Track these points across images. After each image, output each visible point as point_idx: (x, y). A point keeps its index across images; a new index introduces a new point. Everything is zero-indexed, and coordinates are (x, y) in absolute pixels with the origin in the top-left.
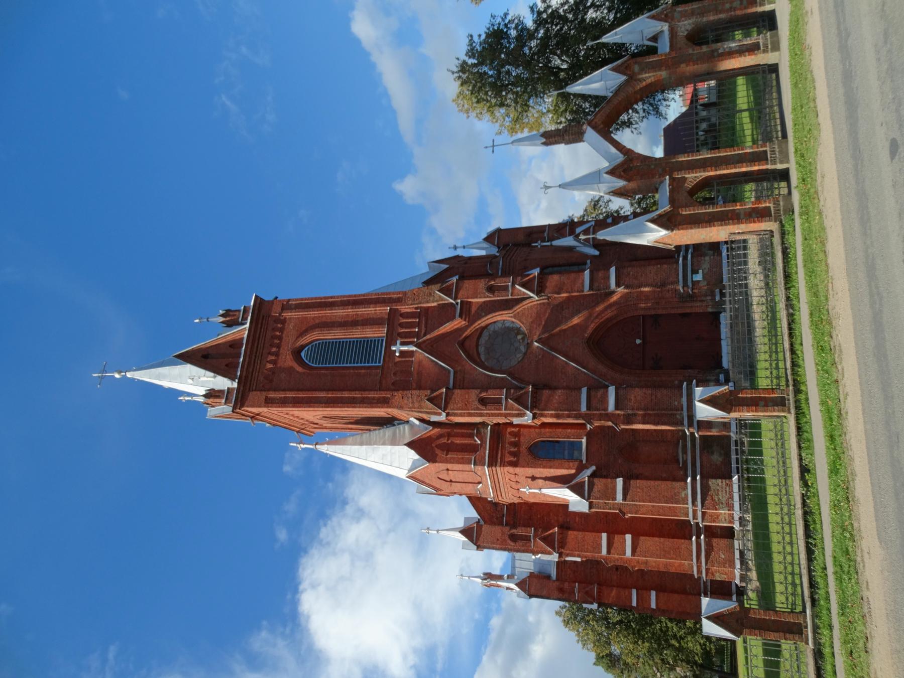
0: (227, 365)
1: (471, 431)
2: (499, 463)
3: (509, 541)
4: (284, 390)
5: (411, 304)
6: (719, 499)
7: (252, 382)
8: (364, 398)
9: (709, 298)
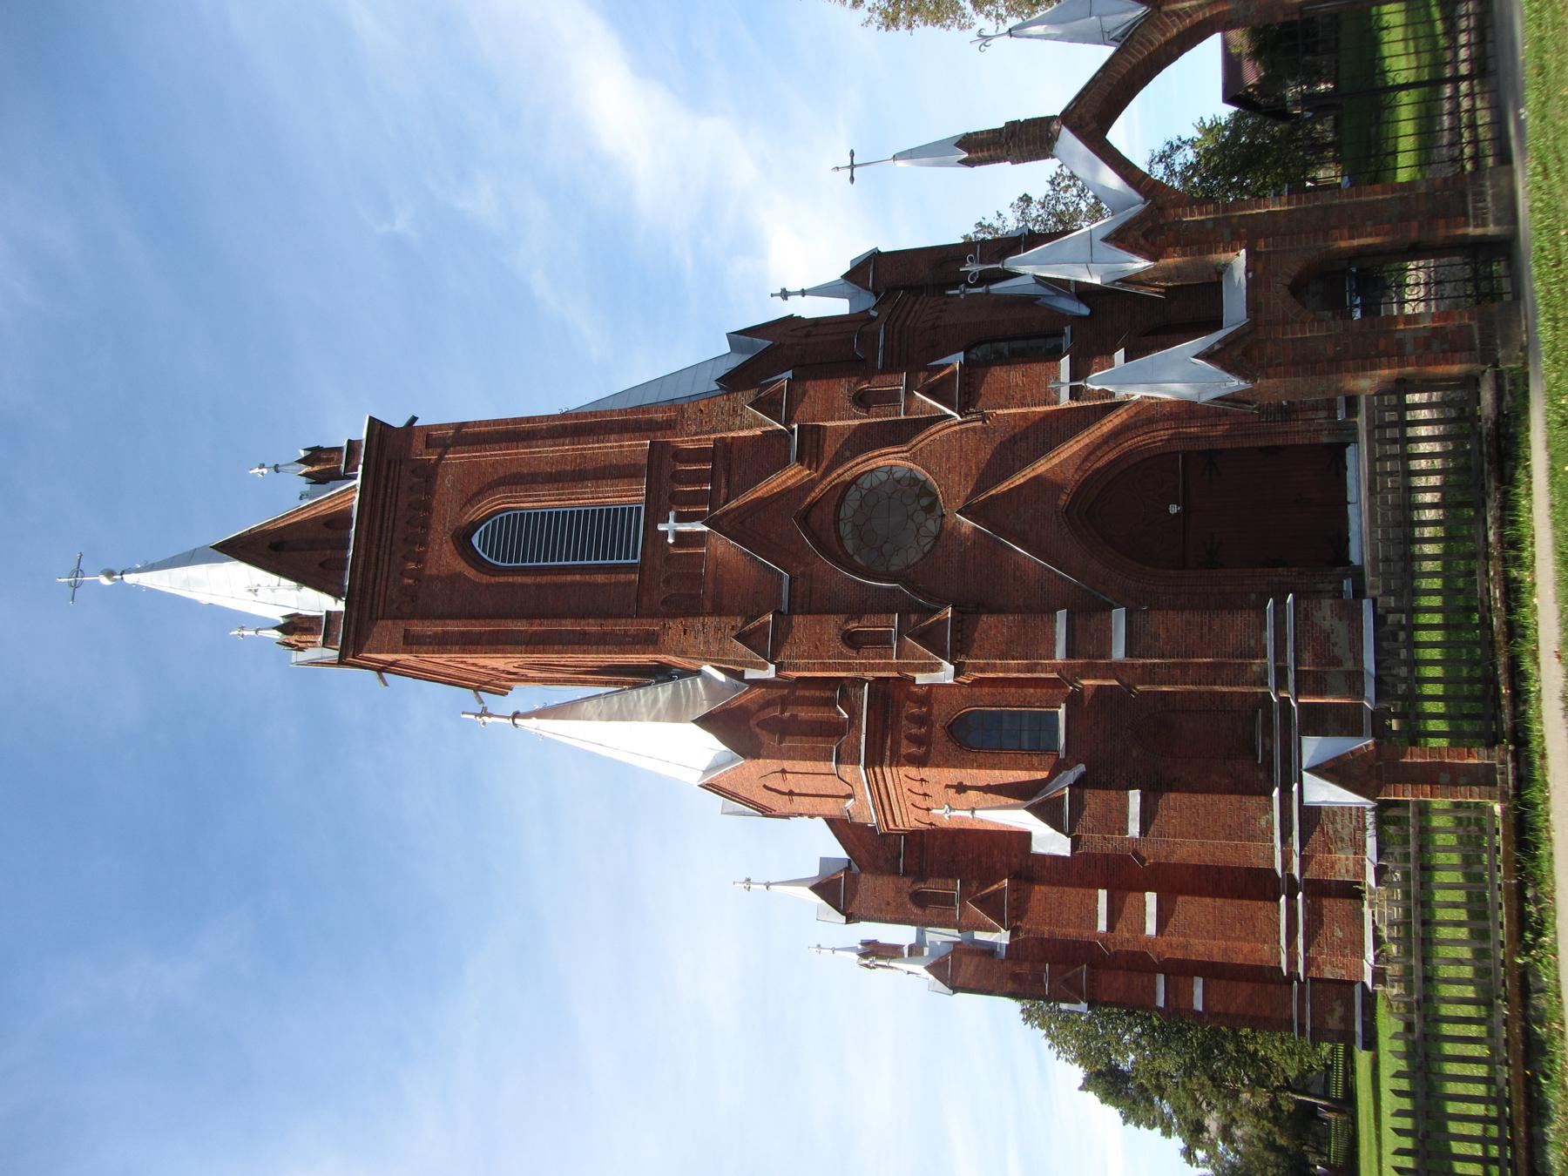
0: (321, 565)
1: (828, 694)
2: (887, 761)
3: (910, 906)
4: (442, 617)
5: (696, 434)
6: (1336, 831)
7: (375, 602)
8: (605, 633)
9: (1323, 414)
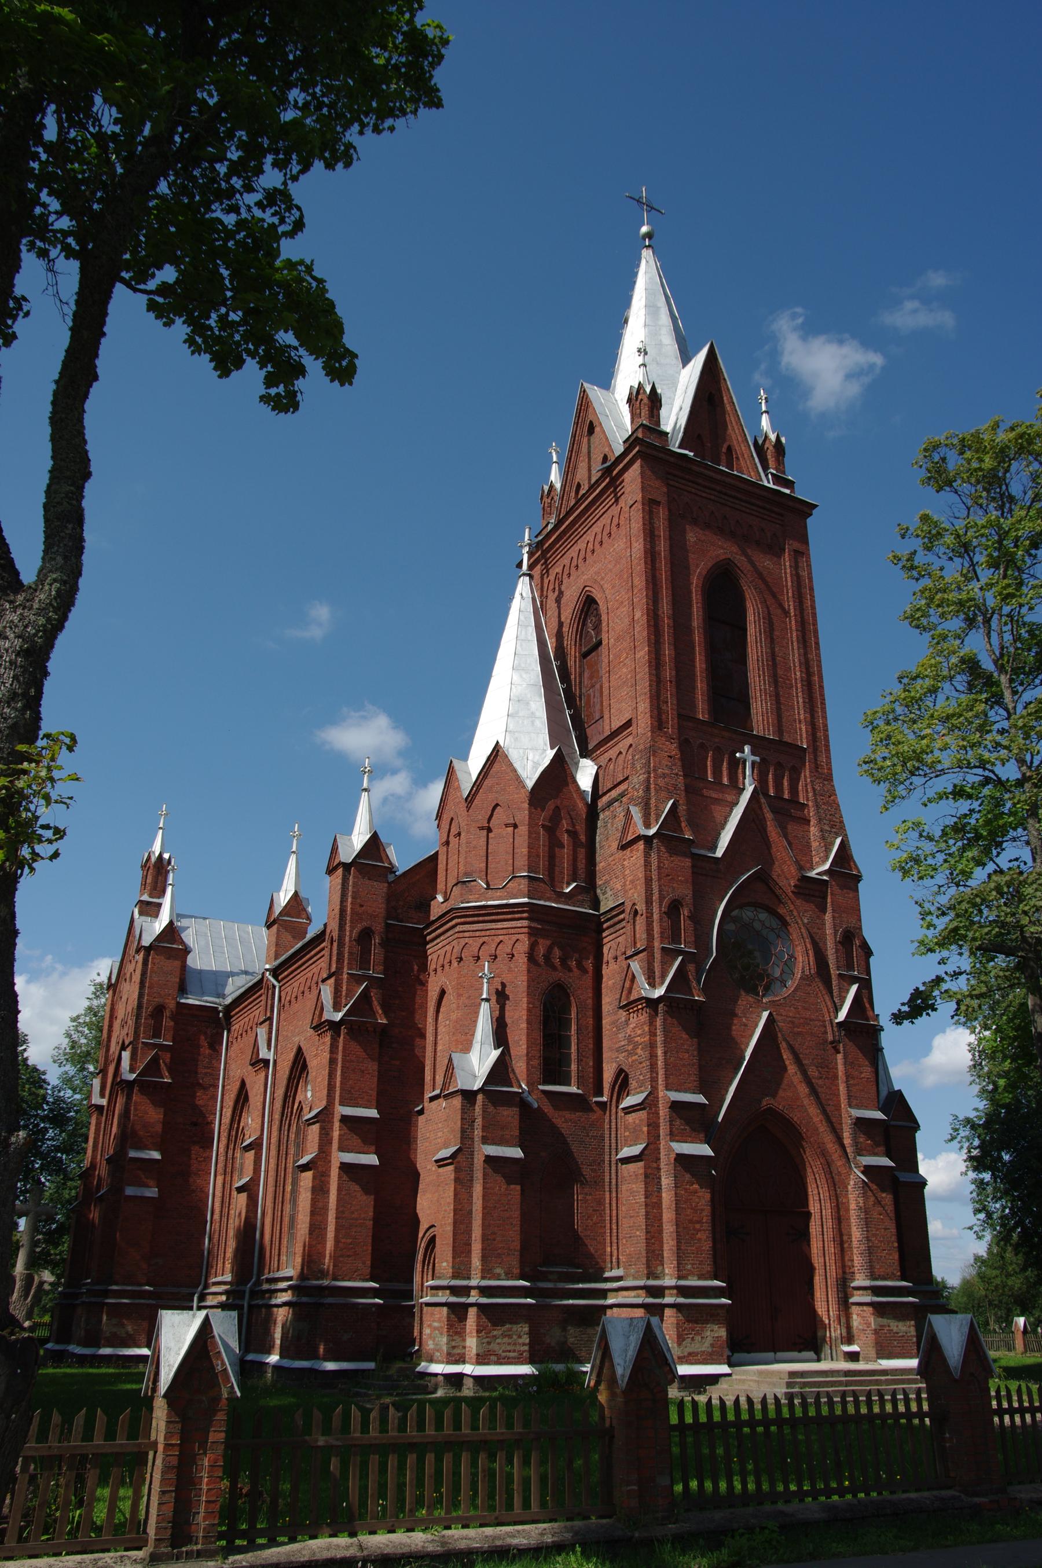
0: (699, 436)
5: (814, 789)
